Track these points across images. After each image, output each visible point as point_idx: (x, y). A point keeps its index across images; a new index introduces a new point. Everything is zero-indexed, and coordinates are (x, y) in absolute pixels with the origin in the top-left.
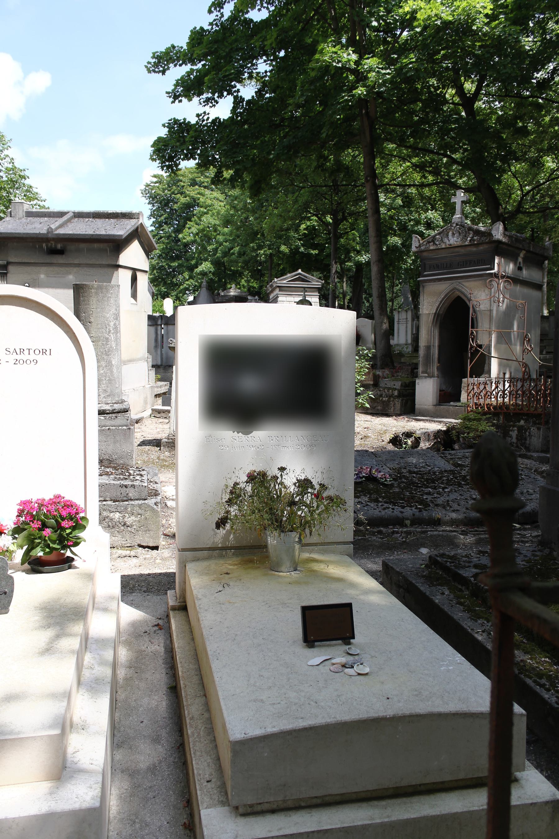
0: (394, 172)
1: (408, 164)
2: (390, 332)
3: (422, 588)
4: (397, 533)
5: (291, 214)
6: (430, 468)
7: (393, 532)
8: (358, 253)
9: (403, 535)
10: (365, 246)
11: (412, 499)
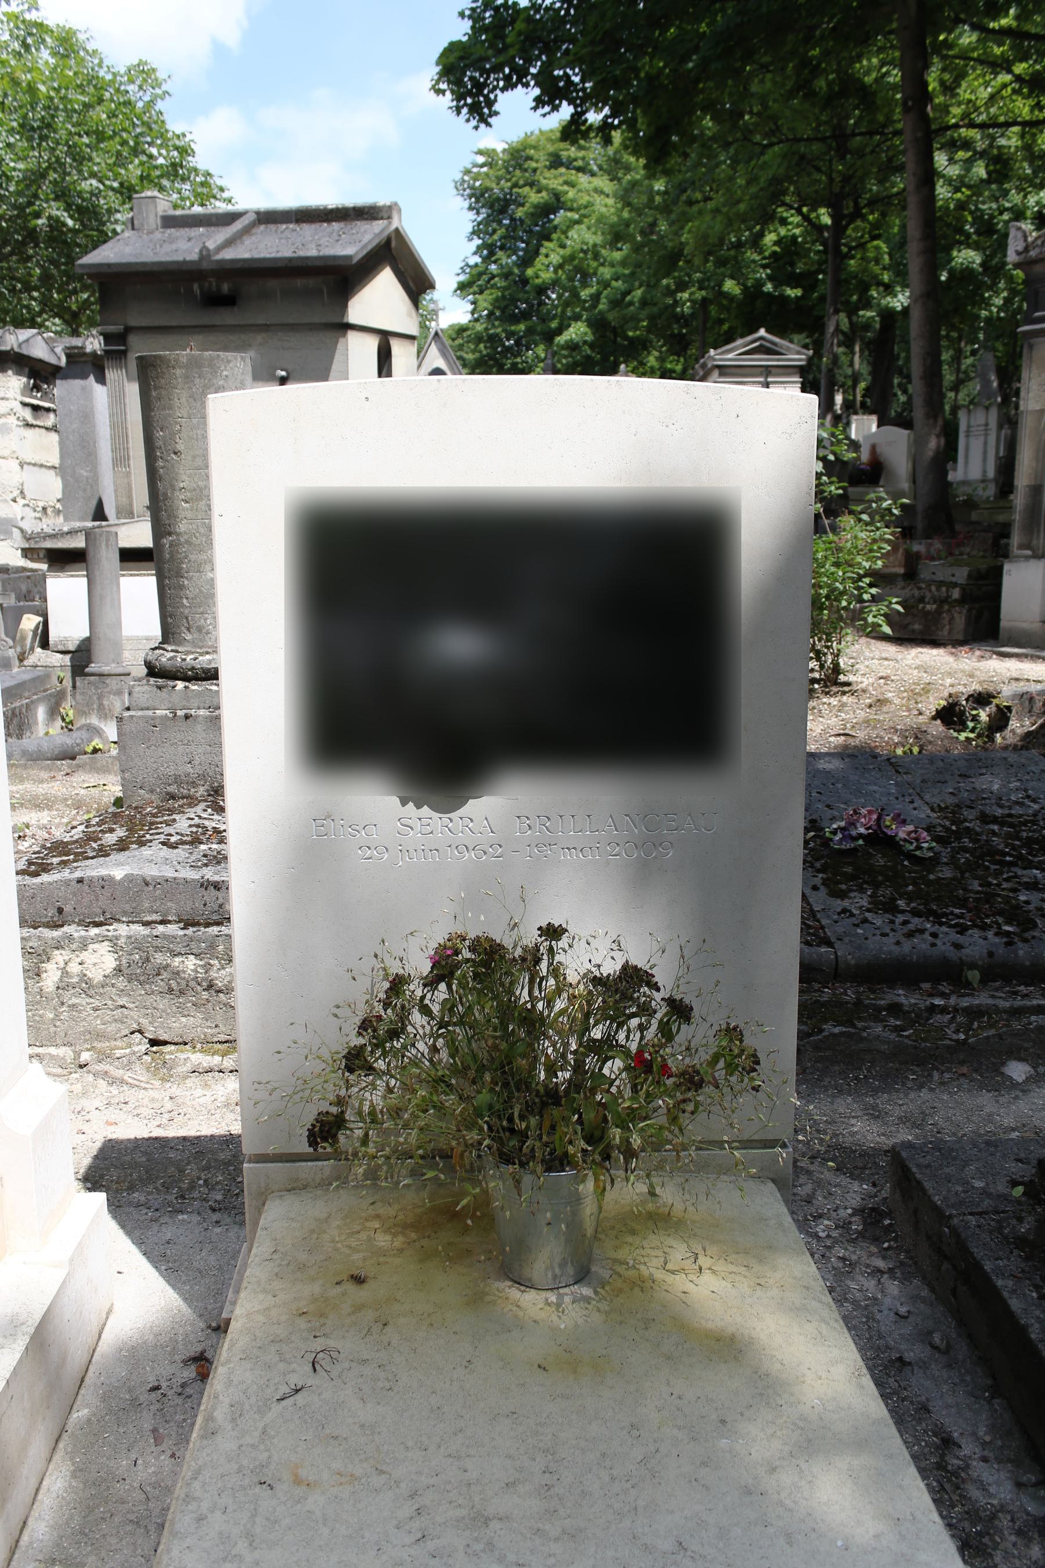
0: (970, 101)
1: (1008, 78)
2: (949, 452)
3: (1015, 1304)
4: (943, 1010)
5: (742, 207)
6: (1036, 807)
7: (933, 1009)
8: (889, 289)
9: (959, 1019)
10: (900, 272)
11: (988, 902)
